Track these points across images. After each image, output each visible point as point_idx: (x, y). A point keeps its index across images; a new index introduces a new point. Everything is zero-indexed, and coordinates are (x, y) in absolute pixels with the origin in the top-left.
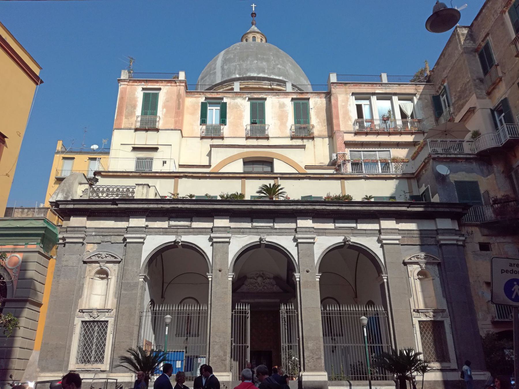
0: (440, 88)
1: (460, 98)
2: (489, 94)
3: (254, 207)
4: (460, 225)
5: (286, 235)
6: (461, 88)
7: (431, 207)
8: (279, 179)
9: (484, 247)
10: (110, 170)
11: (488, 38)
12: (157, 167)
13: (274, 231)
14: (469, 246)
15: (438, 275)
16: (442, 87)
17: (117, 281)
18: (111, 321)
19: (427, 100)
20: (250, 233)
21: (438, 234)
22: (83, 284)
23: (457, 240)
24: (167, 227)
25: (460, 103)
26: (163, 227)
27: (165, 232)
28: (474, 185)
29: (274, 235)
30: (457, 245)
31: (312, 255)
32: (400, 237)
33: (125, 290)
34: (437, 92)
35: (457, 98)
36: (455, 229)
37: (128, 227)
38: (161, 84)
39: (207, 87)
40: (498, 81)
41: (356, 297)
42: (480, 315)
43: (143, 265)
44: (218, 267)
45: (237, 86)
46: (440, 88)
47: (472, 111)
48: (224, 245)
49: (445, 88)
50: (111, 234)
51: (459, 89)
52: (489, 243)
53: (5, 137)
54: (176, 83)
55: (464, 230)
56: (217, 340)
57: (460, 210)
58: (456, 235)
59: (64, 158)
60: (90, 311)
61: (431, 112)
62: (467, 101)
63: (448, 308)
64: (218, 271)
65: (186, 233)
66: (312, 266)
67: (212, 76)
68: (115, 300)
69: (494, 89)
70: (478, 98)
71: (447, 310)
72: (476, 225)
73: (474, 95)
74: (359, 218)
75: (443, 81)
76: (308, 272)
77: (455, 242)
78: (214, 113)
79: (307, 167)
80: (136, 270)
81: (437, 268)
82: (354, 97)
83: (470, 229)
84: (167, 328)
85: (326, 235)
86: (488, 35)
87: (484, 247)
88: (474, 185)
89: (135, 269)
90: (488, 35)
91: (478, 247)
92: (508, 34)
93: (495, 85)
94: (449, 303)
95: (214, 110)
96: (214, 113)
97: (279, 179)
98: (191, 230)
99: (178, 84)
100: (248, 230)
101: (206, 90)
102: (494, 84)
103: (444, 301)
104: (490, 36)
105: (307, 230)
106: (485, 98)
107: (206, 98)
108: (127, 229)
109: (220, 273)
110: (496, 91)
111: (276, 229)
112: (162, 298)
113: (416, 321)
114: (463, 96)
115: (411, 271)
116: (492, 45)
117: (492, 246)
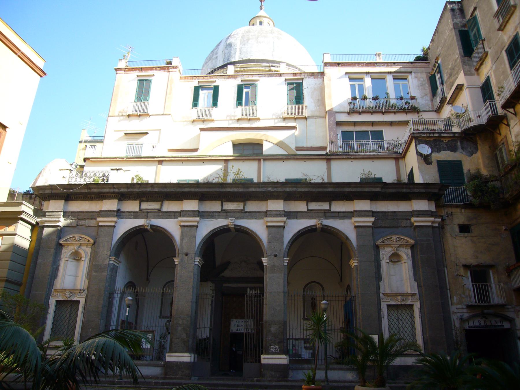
0: (434, 66)
1: (451, 75)
2: (477, 70)
3: (222, 190)
4: (437, 206)
5: (256, 219)
6: (452, 65)
7: (406, 188)
8: (262, 160)
9: (464, 229)
10: (142, 156)
11: (476, 12)
12: (146, 152)
13: (244, 214)
14: (448, 228)
15: (411, 258)
16: (437, 65)
17: (90, 264)
18: (82, 301)
19: (423, 78)
20: (219, 217)
21: (412, 216)
22: (59, 266)
23: (433, 222)
24: (220, 210)
25: (451, 80)
26: (134, 210)
27: (135, 215)
28: (458, 164)
29: (243, 218)
30: (433, 227)
31: (112, 236)
32: (373, 219)
33: (96, 271)
34: (433, 70)
35: (448, 76)
36: (431, 211)
37: (181, 211)
38: (155, 71)
39: (209, 71)
40: (484, 57)
41: (341, 281)
42: (455, 299)
43: (113, 247)
44: (185, 251)
45: (231, 69)
46: (434, 66)
47: (460, 88)
48: (185, 228)
49: (439, 65)
50: (85, 217)
51: (450, 67)
52: (470, 225)
53: (4, 127)
54: (169, 69)
55: (443, 212)
56: (180, 322)
57: (436, 191)
58: (432, 216)
59: (202, 129)
60: (63, 291)
61: (428, 89)
62: (457, 78)
63: (419, 292)
64: (184, 255)
65: (155, 217)
66: (280, 250)
67: (214, 61)
68: (87, 281)
69: (482, 64)
70: (465, 74)
71: (418, 294)
72: (457, 206)
73: (462, 71)
74: (333, 200)
75: (437, 59)
76: (276, 256)
77: (430, 224)
78: (205, 96)
79: (298, 149)
80: (106, 253)
81: (410, 251)
82: (347, 77)
83: (450, 210)
84: (128, 309)
85: (297, 219)
86: (475, 9)
87: (464, 229)
88: (458, 164)
89: (105, 251)
90: (475, 9)
91: (457, 229)
92: (491, 8)
93: (482, 61)
94: (419, 286)
95: (401, 85)
96: (205, 96)
97: (262, 160)
98: (160, 214)
99: (170, 70)
100: (217, 214)
101: (209, 73)
102: (481, 59)
103: (416, 285)
104: (477, 10)
105: (278, 213)
106: (473, 75)
107: (242, 81)
108: (266, 212)
109: (186, 257)
110: (483, 67)
111: (247, 212)
112: (147, 280)
113: (384, 306)
114: (453, 75)
115: (383, 254)
116: (479, 19)
117: (472, 227)
